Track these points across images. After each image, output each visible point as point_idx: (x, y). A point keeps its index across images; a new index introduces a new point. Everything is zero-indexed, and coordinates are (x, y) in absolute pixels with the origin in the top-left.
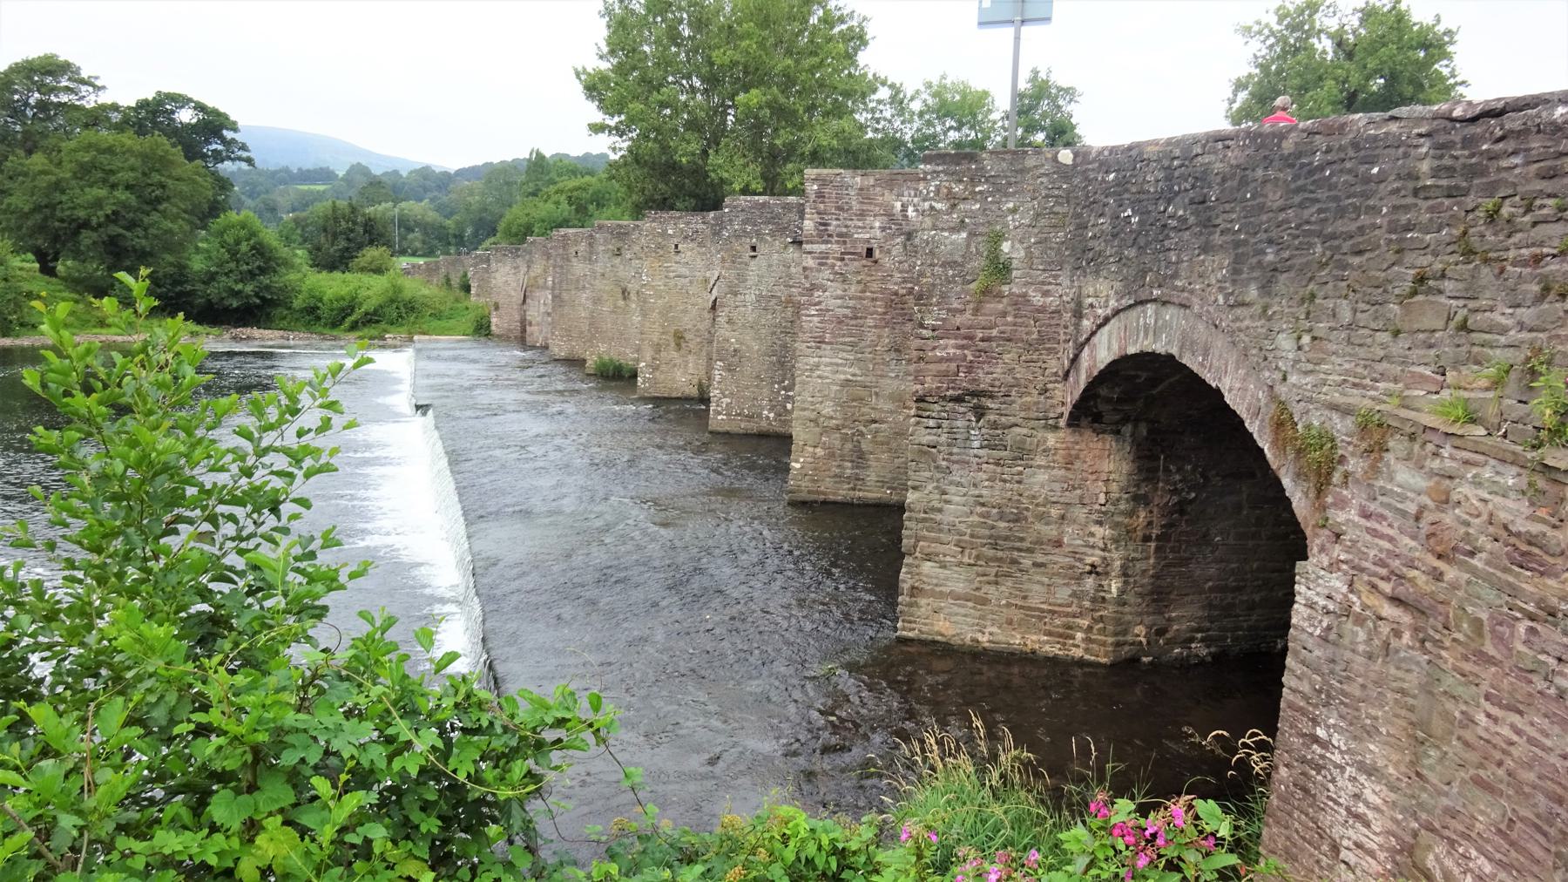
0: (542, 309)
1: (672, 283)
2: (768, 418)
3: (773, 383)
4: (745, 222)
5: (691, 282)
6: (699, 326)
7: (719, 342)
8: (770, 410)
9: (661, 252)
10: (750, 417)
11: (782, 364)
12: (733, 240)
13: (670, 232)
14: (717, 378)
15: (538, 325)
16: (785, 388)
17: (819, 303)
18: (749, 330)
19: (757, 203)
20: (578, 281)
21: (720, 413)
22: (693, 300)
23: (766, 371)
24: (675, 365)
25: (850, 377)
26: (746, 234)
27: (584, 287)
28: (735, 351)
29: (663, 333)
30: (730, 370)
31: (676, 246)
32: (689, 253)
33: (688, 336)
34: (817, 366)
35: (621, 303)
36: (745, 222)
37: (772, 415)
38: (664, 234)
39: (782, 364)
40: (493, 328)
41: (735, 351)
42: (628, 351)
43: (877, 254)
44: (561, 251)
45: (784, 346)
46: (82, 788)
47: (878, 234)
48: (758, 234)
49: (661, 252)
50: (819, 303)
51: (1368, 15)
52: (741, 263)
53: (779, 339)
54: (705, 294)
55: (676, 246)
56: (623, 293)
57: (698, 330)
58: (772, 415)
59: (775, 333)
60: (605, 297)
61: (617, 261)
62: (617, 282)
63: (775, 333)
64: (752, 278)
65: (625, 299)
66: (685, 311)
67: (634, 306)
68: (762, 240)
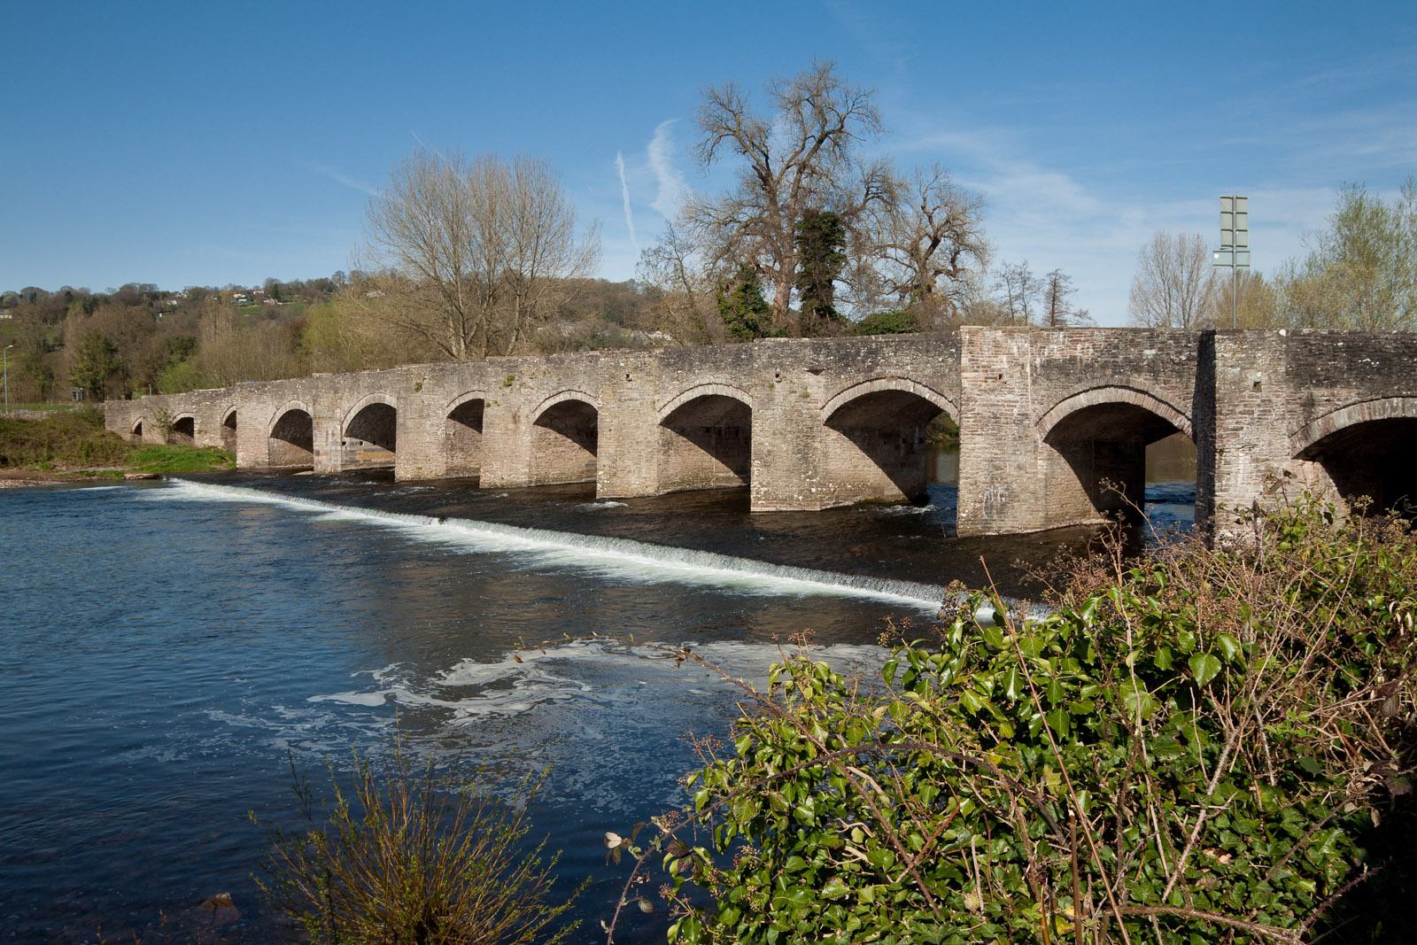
3: (800, 474)
6: (650, 438)
8: (799, 494)
9: (615, 381)
10: (784, 501)
13: (622, 364)
14: (756, 473)
15: (326, 454)
16: (808, 477)
17: (973, 410)
19: (780, 343)
21: (759, 499)
24: (629, 472)
27: (429, 415)
28: (769, 451)
29: (617, 446)
31: (628, 376)
32: (639, 381)
34: (973, 449)
35: (511, 426)
37: (801, 498)
38: (617, 367)
41: (769, 451)
42: (519, 466)
43: (1005, 378)
46: (1231, 700)
47: (1006, 366)
48: (781, 365)
49: (615, 381)
50: (973, 410)
55: (628, 376)
56: (514, 417)
57: (649, 442)
58: (801, 498)
59: (798, 437)
61: (508, 390)
62: (509, 408)
63: (798, 437)
64: (779, 398)
65: (515, 422)
66: (637, 427)
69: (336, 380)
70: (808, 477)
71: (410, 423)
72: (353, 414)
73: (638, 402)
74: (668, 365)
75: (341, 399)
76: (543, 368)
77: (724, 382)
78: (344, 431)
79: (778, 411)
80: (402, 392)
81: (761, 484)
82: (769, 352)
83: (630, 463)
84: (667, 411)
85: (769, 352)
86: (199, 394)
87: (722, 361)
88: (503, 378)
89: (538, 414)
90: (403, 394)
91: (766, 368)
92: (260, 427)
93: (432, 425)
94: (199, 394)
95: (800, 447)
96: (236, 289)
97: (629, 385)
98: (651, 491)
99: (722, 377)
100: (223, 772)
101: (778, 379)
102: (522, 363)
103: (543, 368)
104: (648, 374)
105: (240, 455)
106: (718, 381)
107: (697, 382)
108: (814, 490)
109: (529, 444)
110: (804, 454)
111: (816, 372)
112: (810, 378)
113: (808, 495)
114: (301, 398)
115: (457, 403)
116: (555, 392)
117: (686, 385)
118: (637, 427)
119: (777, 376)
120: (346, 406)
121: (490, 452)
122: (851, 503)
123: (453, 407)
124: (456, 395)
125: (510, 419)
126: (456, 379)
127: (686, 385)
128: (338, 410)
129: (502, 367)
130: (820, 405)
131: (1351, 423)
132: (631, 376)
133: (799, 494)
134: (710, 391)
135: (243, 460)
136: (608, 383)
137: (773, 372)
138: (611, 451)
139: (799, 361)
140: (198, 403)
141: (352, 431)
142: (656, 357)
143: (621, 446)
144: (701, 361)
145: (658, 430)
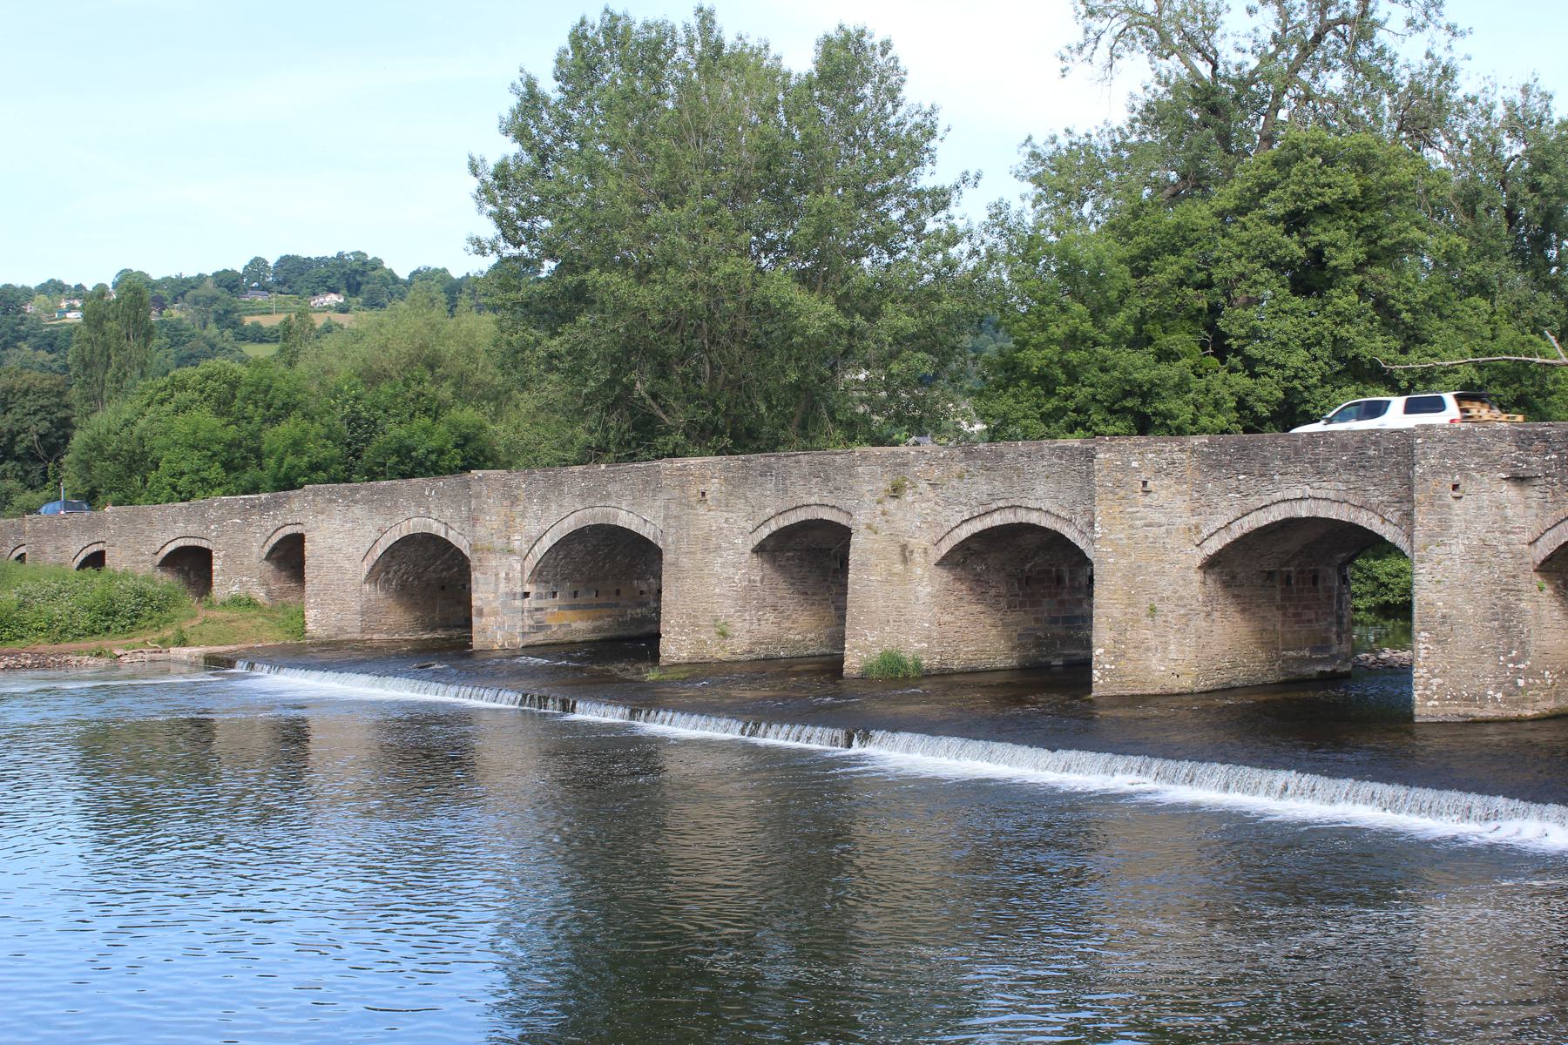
0: (503, 587)
1: (1140, 534)
2: (1494, 699)
4: (1443, 456)
5: (1168, 532)
6: (1182, 592)
7: (1421, 606)
8: (1497, 690)
9: (1122, 493)
10: (1470, 700)
11: (1506, 629)
12: (1429, 477)
13: (1135, 464)
14: (1423, 653)
16: (1512, 660)
18: (1460, 590)
20: (707, 539)
21: (1429, 698)
22: (1173, 556)
23: (1487, 640)
24: (1148, 649)
25: (195, 716)
26: (1446, 470)
30: (1439, 642)
31: (1145, 483)
33: (1163, 608)
35: (898, 568)
36: (1443, 456)
37: (1499, 696)
38: (1126, 468)
39: (1506, 629)
40: (310, 627)
41: (1444, 617)
44: (677, 493)
45: (1507, 608)
48: (1461, 469)
49: (1122, 493)
51: (760, 40)
52: (1441, 506)
53: (1500, 598)
54: (1191, 549)
55: (1145, 483)
57: (1181, 598)
58: (1499, 696)
60: (873, 559)
61: (891, 505)
64: (1457, 525)
65: (905, 560)
67: (919, 571)
68: (1468, 477)
69: (514, 483)
70: (1512, 660)
71: (685, 561)
72: (547, 543)
73: (1163, 529)
74: (1218, 465)
75: (523, 516)
76: (958, 467)
77: (1332, 495)
78: (527, 575)
79: (1458, 548)
80: (673, 507)
81: (1430, 671)
82: (1440, 448)
83: (1149, 634)
84: (1214, 545)
85: (1440, 448)
86: (221, 506)
87: (1328, 460)
88: (884, 485)
89: (945, 548)
90: (674, 510)
91: (1435, 473)
92: (347, 565)
93: (723, 565)
94: (221, 506)
95: (1498, 609)
96: (54, 288)
97: (1147, 500)
98: (1186, 683)
99: (1329, 488)
100: (1338, 897)
101: (1456, 494)
102: (916, 459)
103: (958, 467)
104: (1179, 481)
105: (311, 614)
106: (1319, 494)
107: (1278, 496)
108: (1521, 683)
109: (927, 599)
110: (1506, 622)
111: (1519, 480)
112: (1509, 492)
113: (1513, 693)
114: (435, 515)
115: (773, 526)
116: (982, 510)
117: (1254, 501)
118: (1161, 573)
119: (1455, 487)
120: (534, 528)
121: (861, 613)
122: (1529, 713)
123: (765, 532)
124: (770, 511)
125: (896, 557)
126: (771, 486)
127: (1254, 501)
128: (517, 537)
129: (882, 465)
130: (1528, 537)
131: (722, 655)
132: (1150, 483)
133: (1497, 690)
134: (1303, 511)
135: (318, 620)
136: (1110, 496)
137: (1448, 480)
138: (1116, 613)
139: (1492, 464)
140: (220, 520)
141: (540, 574)
142: (1193, 451)
143: (1134, 605)
144: (1286, 459)
145: (1197, 577)
